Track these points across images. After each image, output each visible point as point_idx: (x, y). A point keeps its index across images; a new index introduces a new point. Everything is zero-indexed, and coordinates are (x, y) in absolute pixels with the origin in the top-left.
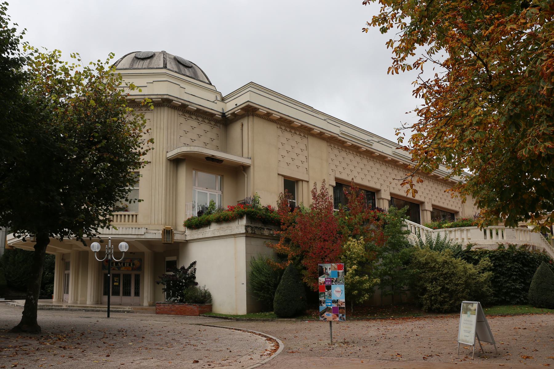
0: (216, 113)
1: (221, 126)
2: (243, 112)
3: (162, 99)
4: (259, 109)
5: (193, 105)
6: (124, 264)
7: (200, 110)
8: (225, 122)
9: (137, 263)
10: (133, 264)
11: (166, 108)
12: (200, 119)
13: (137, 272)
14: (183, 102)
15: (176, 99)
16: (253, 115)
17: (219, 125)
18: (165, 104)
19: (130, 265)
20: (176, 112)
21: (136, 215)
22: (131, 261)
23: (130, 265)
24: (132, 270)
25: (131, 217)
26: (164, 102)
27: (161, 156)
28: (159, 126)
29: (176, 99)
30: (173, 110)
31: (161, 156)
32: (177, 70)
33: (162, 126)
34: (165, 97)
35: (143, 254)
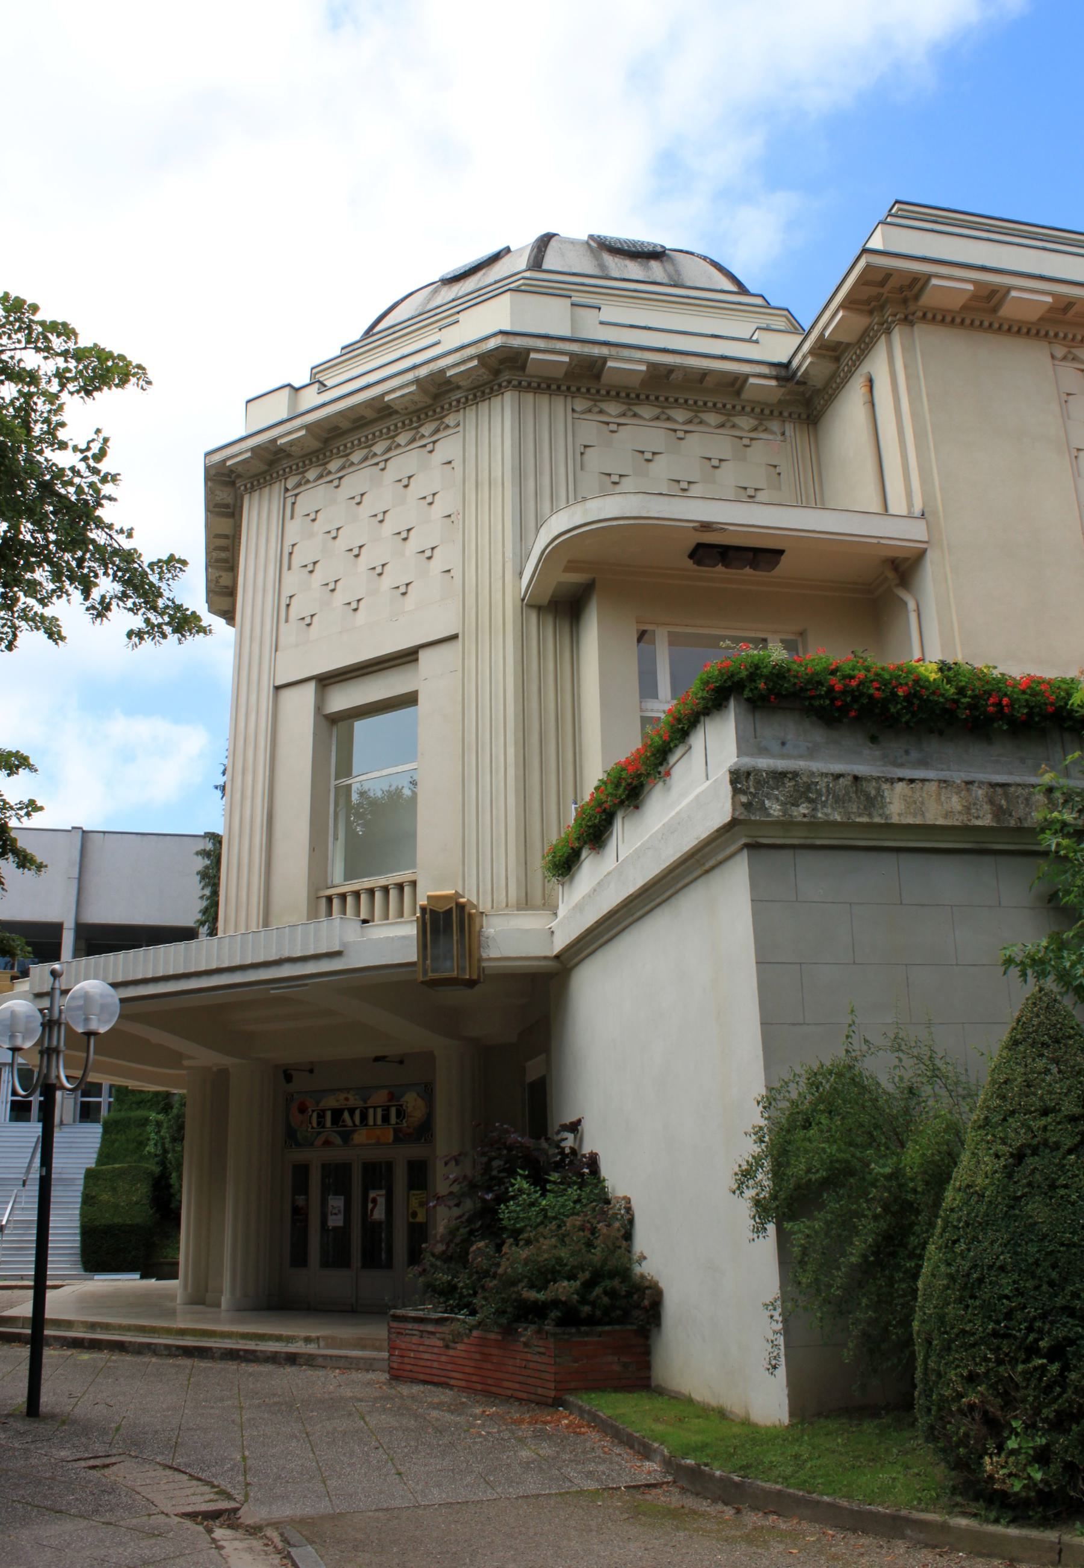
0: (746, 368)
1: (789, 428)
2: (860, 322)
3: (481, 357)
4: (929, 277)
5: (626, 353)
6: (364, 1117)
7: (670, 370)
8: (801, 401)
9: (412, 1102)
10: (400, 1114)
11: (509, 397)
12: (680, 415)
13: (414, 1151)
14: (575, 348)
15: (541, 344)
16: (908, 321)
17: (775, 426)
18: (505, 376)
19: (386, 1119)
20: (559, 403)
21: (414, 884)
22: (392, 1096)
23: (386, 1119)
24: (397, 1140)
25: (393, 893)
26: (497, 373)
27: (498, 597)
28: (484, 476)
29: (541, 344)
30: (544, 400)
31: (498, 597)
32: (600, 274)
33: (497, 473)
34: (492, 344)
35: (428, 1058)
